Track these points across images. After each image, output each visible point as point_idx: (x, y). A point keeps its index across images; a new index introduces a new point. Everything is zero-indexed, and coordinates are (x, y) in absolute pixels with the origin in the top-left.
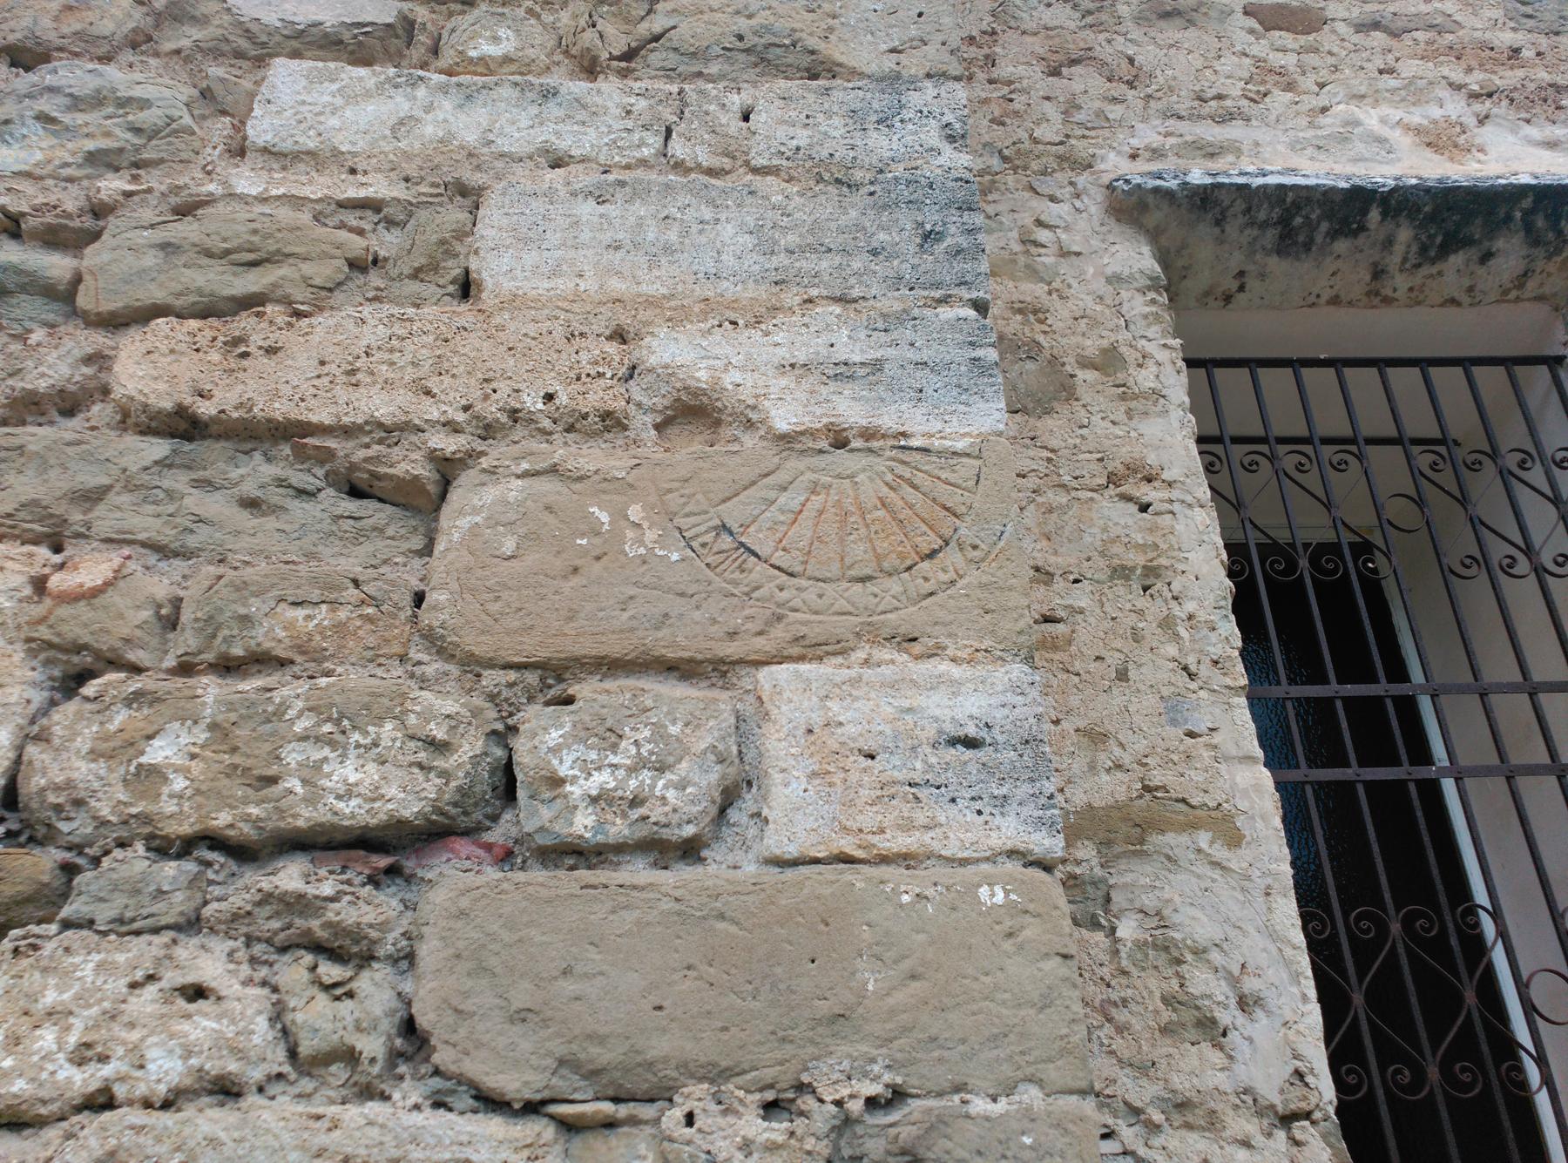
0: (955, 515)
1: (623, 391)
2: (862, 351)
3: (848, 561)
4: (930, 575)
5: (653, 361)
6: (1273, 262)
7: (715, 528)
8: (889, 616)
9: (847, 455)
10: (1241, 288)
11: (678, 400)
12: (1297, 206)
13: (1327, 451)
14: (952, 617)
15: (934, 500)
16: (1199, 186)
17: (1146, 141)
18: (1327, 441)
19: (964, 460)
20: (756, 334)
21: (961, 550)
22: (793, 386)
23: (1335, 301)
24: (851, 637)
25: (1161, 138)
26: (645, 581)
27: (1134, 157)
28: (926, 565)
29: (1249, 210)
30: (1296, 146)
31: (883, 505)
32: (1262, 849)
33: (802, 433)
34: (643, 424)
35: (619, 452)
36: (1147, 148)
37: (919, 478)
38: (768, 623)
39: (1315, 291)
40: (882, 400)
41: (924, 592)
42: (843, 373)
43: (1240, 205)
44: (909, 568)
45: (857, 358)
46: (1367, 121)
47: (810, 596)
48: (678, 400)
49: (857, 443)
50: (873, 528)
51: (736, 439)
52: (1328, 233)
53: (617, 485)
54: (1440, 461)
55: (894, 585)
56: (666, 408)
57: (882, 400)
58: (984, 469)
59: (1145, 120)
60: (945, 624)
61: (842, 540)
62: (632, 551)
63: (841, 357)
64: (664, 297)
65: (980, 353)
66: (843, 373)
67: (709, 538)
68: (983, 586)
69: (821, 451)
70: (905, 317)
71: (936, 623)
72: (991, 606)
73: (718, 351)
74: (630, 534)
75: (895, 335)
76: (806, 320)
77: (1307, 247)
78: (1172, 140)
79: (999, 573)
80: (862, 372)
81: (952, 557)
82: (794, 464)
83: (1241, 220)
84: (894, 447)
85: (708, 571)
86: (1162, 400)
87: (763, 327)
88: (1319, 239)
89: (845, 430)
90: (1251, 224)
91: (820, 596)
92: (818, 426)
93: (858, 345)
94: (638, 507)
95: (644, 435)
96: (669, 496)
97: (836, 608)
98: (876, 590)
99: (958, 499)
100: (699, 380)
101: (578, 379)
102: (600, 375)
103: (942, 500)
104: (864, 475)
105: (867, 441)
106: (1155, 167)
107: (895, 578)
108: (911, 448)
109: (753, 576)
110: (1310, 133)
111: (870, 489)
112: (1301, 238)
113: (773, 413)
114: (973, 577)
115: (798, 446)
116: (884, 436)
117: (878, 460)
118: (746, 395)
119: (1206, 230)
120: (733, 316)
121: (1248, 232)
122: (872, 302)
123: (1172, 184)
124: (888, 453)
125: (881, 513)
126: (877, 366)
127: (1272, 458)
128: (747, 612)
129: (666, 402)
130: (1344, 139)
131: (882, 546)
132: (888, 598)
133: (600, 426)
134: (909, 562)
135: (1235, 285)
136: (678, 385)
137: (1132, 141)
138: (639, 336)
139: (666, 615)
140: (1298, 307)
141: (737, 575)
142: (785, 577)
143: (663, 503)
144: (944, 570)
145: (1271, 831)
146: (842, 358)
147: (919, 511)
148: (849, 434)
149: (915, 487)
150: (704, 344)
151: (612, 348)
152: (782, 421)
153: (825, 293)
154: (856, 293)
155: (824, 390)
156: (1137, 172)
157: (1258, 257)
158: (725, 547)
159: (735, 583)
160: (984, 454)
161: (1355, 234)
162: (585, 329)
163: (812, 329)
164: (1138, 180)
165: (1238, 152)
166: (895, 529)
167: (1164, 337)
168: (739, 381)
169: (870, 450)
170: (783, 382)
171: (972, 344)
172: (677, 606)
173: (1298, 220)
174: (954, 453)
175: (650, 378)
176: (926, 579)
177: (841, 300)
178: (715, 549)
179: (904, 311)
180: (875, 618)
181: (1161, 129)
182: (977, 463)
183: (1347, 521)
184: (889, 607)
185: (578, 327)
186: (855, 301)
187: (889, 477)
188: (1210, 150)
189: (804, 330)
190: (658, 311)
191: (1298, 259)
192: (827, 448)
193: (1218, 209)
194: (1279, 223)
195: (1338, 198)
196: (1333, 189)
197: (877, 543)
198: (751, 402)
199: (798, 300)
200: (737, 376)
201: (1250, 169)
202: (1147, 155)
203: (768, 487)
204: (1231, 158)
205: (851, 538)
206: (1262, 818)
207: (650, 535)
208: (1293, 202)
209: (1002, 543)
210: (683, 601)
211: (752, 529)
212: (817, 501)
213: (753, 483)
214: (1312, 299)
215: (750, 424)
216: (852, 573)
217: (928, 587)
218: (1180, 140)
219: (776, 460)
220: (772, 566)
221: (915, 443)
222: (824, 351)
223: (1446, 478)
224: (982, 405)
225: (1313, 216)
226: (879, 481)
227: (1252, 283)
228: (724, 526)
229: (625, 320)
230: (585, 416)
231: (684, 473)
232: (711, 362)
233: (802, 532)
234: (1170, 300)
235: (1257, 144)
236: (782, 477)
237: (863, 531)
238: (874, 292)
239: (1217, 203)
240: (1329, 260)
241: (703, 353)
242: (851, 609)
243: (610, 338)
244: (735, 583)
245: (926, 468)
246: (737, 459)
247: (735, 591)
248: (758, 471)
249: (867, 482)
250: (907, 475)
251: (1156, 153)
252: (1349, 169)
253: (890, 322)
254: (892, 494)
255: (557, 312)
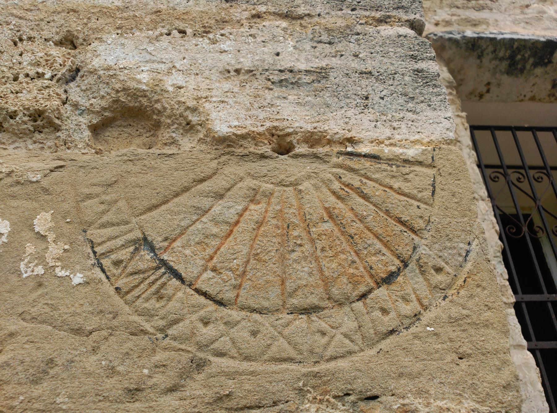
1: (61, 91)
2: (307, 60)
3: (290, 285)
4: (389, 305)
5: (96, 63)
6: (505, 79)
7: (134, 242)
8: (342, 363)
9: (291, 161)
10: (488, 91)
12: (519, 50)
13: (532, 173)
14: (419, 366)
15: (387, 212)
16: (471, 38)
17: (443, 18)
18: (532, 168)
19: (417, 168)
20: (204, 43)
21: (423, 273)
22: (236, 90)
23: (533, 99)
24: (292, 395)
25: (449, 17)
26: (34, 311)
27: (437, 24)
28: (382, 292)
29: (495, 51)
30: (515, 22)
31: (331, 216)
32: (533, 404)
33: (243, 137)
34: (78, 126)
35: (47, 153)
36: (443, 21)
37: (370, 187)
38: (185, 374)
39: (524, 93)
40: (328, 106)
41: (384, 329)
42: (288, 79)
43: (491, 49)
44: (363, 296)
45: (302, 66)
46: (549, 12)
47: (241, 333)
48: (117, 101)
49: (301, 149)
50: (319, 245)
51: (173, 142)
52: (532, 64)
53: (29, 189)
54: (521, 176)
55: (345, 319)
56: (104, 109)
57: (328, 106)
58: (439, 179)
59: (441, 8)
60: (411, 376)
61: (283, 258)
62: (29, 269)
63: (286, 64)
64: (118, 9)
66: (288, 79)
68: (454, 321)
69: (263, 157)
70: (346, 33)
71: (401, 375)
73: (164, 56)
74: (30, 248)
75: (339, 47)
76: (253, 31)
78: (454, 18)
79: (470, 304)
80: (307, 79)
82: (234, 169)
84: (340, 153)
85: (117, 299)
86: (458, 144)
87: (211, 36)
88: (528, 67)
89: (289, 134)
90: (496, 58)
91: (254, 333)
92: (261, 129)
93: (304, 55)
94: (48, 216)
95: (76, 137)
96: (88, 203)
97: (273, 351)
98: (324, 325)
100: (139, 82)
101: (16, 79)
102: (40, 76)
103: (396, 212)
104: (310, 184)
105: (311, 147)
106: (448, 29)
107: (347, 309)
108: (359, 155)
109: (173, 305)
110: (522, 17)
111: (316, 199)
112: (519, 66)
113: (213, 115)
114: (439, 310)
115: (239, 151)
116: (330, 142)
117: (323, 167)
119: (473, 61)
120: (182, 25)
121: (494, 62)
122: (316, 19)
123: (458, 37)
124: (334, 160)
125: (328, 226)
126: (322, 74)
127: (505, 175)
128: (160, 356)
129: (104, 103)
130: (539, 19)
131: (331, 267)
132: (339, 337)
133: (30, 126)
134: (363, 289)
135: (485, 90)
136: (118, 86)
137: (435, 17)
138: (87, 41)
139: (51, 362)
140: (522, 100)
141: (152, 304)
142: (212, 306)
144: (405, 299)
145: (537, 393)
146: (288, 65)
148: (293, 139)
149: (365, 197)
150: (150, 48)
151: (56, 52)
152: (223, 123)
153: (272, 9)
154: (302, 10)
155: (268, 95)
156: (440, 31)
157: (498, 75)
158: (142, 266)
159: (148, 315)
160: (438, 163)
161: (546, 64)
162: (32, 34)
163: (259, 39)
164: (441, 34)
165: (488, 24)
166: (345, 245)
167: (457, 111)
168: (180, 83)
169: (316, 156)
170: (227, 86)
171: (413, 57)
172: (65, 346)
173: (519, 57)
174: (406, 161)
175: (90, 79)
176: (385, 311)
177: (286, 16)
178: (130, 269)
179: (348, 26)
180: (323, 367)
181: (449, 13)
182: (431, 172)
184: (342, 350)
185: (27, 31)
186: (301, 17)
187: (336, 186)
188: (474, 23)
189: (251, 39)
190: (111, 20)
191: (517, 77)
195: (539, 46)
196: (538, 42)
197: (324, 263)
198: (191, 103)
199: (246, 14)
200: (179, 79)
201: (495, 31)
202: (444, 24)
204: (484, 26)
205: (294, 256)
206: (531, 384)
207: (55, 250)
208: (517, 48)
209: (469, 266)
211: (178, 243)
212: (256, 210)
213: (186, 189)
214: (522, 97)
216: (294, 301)
217: (388, 321)
218: (459, 18)
219: (214, 164)
220: (198, 291)
221: (363, 149)
222: (270, 59)
223: (525, 186)
224: (429, 113)
225: (526, 55)
226: (325, 190)
227: (493, 88)
228: (145, 239)
229: (75, 25)
230: (13, 115)
231: (108, 176)
232: (155, 66)
234: (457, 93)
235: (496, 21)
236: (218, 183)
237: (308, 247)
238: (318, 10)
239: (479, 47)
240: (532, 78)
241: (148, 57)
242: (293, 353)
243: (59, 43)
244: (148, 315)
245: (377, 176)
246: (172, 163)
247: (148, 327)
248: (192, 176)
249: (312, 190)
250: (357, 184)
251: (448, 23)
252: (543, 33)
253: (333, 37)
254: (340, 205)
255: (10, 19)
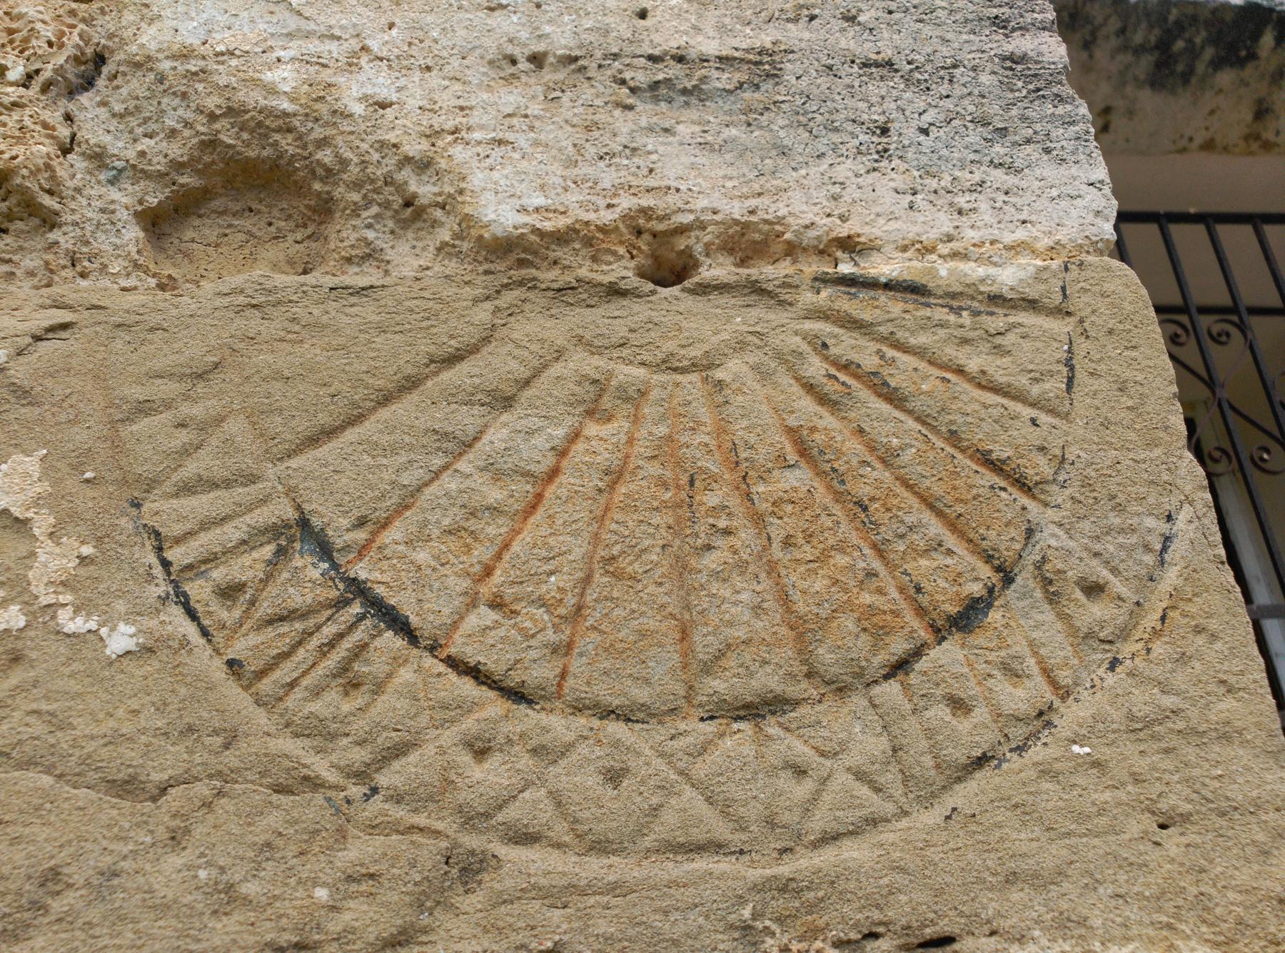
0: (1023, 485)
1: (54, 116)
3: (705, 643)
4: (971, 689)
5: (150, 39)
7: (275, 531)
8: (852, 852)
9: (689, 302)
11: (211, 144)
13: (1205, 321)
14: (1056, 852)
15: (953, 437)
18: (1204, 310)
21: (1053, 599)
22: (535, 109)
23: (1209, 146)
29: (1122, 31)
31: (803, 452)
33: (560, 238)
34: (105, 213)
37: (905, 372)
41: (959, 755)
44: (900, 667)
45: (710, 46)
47: (579, 777)
48: (211, 144)
49: (717, 269)
50: (777, 530)
51: (371, 255)
54: (1179, 331)
55: (854, 729)
56: (178, 166)
58: (1082, 346)
60: (1039, 882)
61: (682, 568)
65: (1022, 44)
67: (246, 567)
68: (1139, 727)
69: (615, 291)
71: (1012, 878)
72: (1174, 801)
77: (1186, 78)
80: (723, 79)
81: (1024, 622)
82: (539, 327)
83: (1114, 42)
84: (822, 280)
85: (233, 693)
88: (1200, 67)
89: (682, 230)
90: (1125, 48)
91: (614, 777)
92: (607, 217)
95: (103, 242)
96: (142, 425)
98: (800, 750)
99: (1023, 433)
100: (271, 90)
104: (743, 366)
105: (742, 263)
107: (858, 701)
108: (871, 284)
109: (389, 705)
112: (1180, 68)
113: (477, 179)
115: (550, 276)
116: (792, 250)
117: (778, 316)
118: (405, 133)
125: (798, 479)
126: (763, 66)
129: (176, 150)
131: (810, 589)
132: (842, 779)
134: (898, 646)
136: (212, 102)
139: (52, 878)
141: (332, 703)
142: (495, 706)
143: (117, 446)
144: (1012, 672)
147: (915, 472)
148: (695, 243)
149: (893, 397)
155: (623, 124)
157: (1129, 90)
158: (298, 598)
159: (321, 733)
161: (1241, 63)
168: (385, 93)
169: (757, 289)
170: (510, 98)
171: (999, 23)
173: (1180, 45)
174: (996, 299)
175: (136, 85)
178: (265, 608)
180: (803, 863)
183: (1236, 405)
187: (815, 368)
192: (634, 281)
193: (1089, 27)
194: (1157, 47)
195: (1229, 17)
197: (793, 578)
198: (415, 148)
200: (381, 83)
203: (454, 397)
205: (711, 561)
207: (53, 560)
209: (1171, 577)
210: (119, 811)
211: (388, 536)
212: (602, 437)
213: (411, 384)
214: (1184, 142)
215: (412, 214)
216: (718, 685)
217: (972, 733)
219: (483, 314)
221: (884, 267)
222: (622, 27)
224: (1049, 171)
225: (1198, 40)
226: (786, 380)
228: (304, 523)
231: (194, 351)
232: (313, 46)
233: (557, 540)
236: (496, 365)
237: (746, 536)
241: (293, 23)
242: (722, 830)
244: (321, 733)
245: (921, 339)
246: (368, 311)
247: (322, 767)
249: (751, 381)
250: (869, 362)
254: (828, 420)
